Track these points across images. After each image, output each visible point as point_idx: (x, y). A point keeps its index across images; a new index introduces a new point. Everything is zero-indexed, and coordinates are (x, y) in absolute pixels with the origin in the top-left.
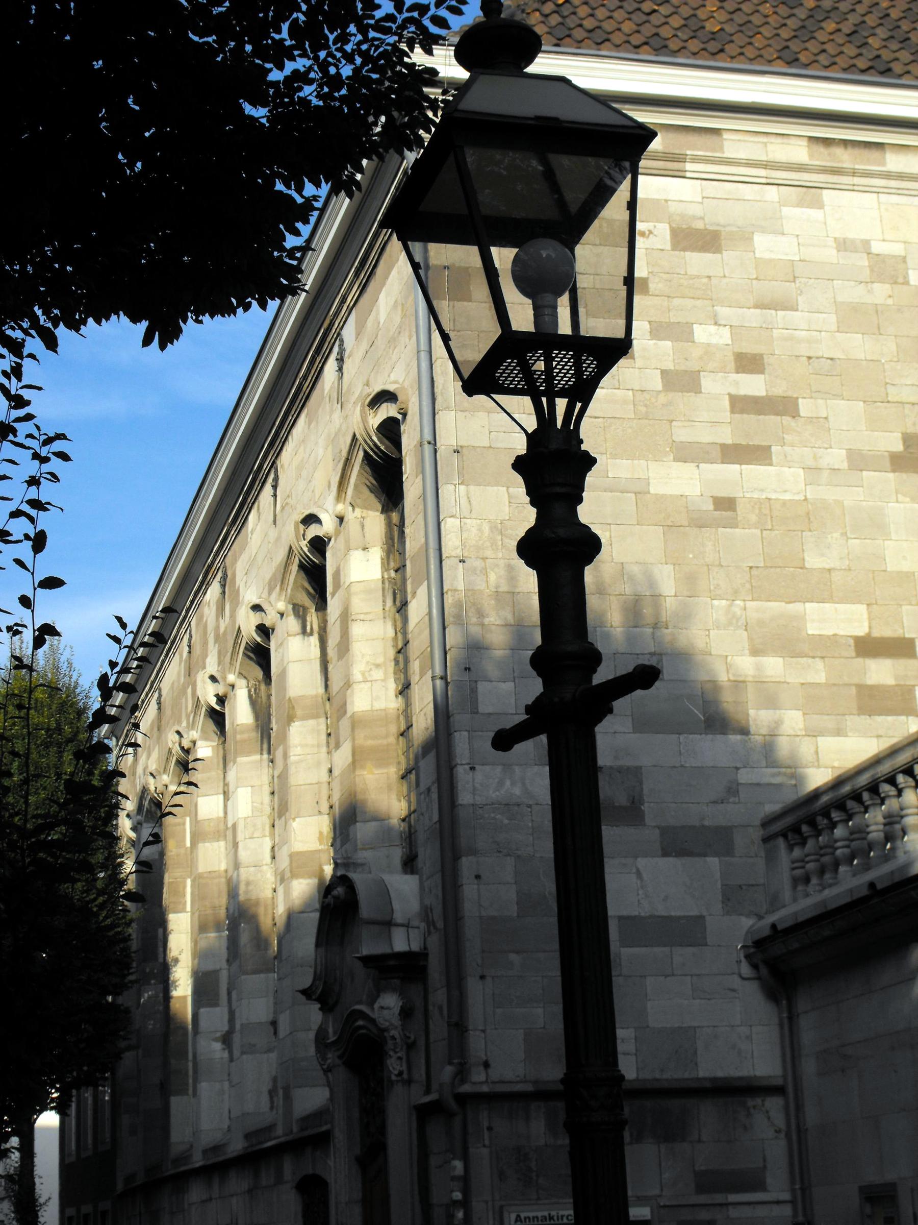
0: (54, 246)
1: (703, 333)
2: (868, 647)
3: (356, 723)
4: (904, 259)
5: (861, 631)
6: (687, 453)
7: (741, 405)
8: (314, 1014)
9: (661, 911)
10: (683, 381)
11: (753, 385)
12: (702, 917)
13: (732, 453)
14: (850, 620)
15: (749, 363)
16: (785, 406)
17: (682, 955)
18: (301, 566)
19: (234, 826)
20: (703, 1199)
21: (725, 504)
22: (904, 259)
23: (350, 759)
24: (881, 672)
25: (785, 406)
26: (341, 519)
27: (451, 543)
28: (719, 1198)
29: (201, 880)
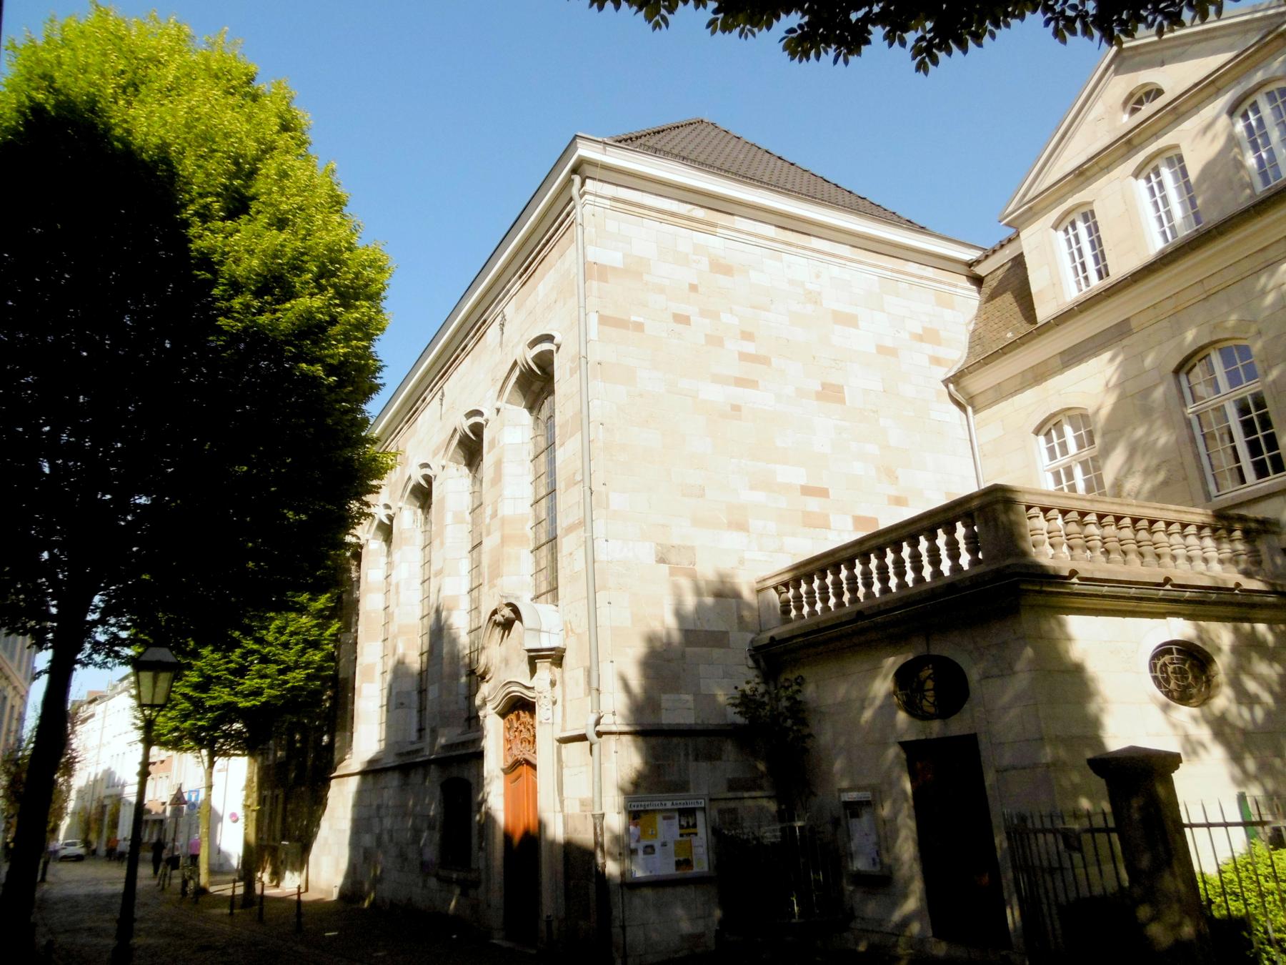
0: (37, 521)
1: (725, 317)
2: (807, 491)
3: (503, 522)
4: (819, 294)
5: (803, 482)
6: (717, 379)
7: (744, 357)
8: (746, 678)
9: (707, 628)
10: (715, 341)
11: (749, 348)
12: (727, 632)
13: (740, 382)
14: (797, 476)
15: (747, 336)
16: (763, 360)
17: (717, 653)
18: (461, 443)
19: (397, 585)
20: (730, 795)
21: (736, 408)
22: (819, 294)
23: (499, 541)
24: (813, 504)
25: (763, 360)
26: (498, 410)
27: (596, 413)
28: (739, 794)
29: (1000, 507)
